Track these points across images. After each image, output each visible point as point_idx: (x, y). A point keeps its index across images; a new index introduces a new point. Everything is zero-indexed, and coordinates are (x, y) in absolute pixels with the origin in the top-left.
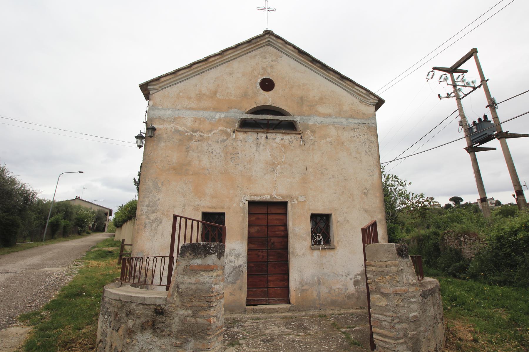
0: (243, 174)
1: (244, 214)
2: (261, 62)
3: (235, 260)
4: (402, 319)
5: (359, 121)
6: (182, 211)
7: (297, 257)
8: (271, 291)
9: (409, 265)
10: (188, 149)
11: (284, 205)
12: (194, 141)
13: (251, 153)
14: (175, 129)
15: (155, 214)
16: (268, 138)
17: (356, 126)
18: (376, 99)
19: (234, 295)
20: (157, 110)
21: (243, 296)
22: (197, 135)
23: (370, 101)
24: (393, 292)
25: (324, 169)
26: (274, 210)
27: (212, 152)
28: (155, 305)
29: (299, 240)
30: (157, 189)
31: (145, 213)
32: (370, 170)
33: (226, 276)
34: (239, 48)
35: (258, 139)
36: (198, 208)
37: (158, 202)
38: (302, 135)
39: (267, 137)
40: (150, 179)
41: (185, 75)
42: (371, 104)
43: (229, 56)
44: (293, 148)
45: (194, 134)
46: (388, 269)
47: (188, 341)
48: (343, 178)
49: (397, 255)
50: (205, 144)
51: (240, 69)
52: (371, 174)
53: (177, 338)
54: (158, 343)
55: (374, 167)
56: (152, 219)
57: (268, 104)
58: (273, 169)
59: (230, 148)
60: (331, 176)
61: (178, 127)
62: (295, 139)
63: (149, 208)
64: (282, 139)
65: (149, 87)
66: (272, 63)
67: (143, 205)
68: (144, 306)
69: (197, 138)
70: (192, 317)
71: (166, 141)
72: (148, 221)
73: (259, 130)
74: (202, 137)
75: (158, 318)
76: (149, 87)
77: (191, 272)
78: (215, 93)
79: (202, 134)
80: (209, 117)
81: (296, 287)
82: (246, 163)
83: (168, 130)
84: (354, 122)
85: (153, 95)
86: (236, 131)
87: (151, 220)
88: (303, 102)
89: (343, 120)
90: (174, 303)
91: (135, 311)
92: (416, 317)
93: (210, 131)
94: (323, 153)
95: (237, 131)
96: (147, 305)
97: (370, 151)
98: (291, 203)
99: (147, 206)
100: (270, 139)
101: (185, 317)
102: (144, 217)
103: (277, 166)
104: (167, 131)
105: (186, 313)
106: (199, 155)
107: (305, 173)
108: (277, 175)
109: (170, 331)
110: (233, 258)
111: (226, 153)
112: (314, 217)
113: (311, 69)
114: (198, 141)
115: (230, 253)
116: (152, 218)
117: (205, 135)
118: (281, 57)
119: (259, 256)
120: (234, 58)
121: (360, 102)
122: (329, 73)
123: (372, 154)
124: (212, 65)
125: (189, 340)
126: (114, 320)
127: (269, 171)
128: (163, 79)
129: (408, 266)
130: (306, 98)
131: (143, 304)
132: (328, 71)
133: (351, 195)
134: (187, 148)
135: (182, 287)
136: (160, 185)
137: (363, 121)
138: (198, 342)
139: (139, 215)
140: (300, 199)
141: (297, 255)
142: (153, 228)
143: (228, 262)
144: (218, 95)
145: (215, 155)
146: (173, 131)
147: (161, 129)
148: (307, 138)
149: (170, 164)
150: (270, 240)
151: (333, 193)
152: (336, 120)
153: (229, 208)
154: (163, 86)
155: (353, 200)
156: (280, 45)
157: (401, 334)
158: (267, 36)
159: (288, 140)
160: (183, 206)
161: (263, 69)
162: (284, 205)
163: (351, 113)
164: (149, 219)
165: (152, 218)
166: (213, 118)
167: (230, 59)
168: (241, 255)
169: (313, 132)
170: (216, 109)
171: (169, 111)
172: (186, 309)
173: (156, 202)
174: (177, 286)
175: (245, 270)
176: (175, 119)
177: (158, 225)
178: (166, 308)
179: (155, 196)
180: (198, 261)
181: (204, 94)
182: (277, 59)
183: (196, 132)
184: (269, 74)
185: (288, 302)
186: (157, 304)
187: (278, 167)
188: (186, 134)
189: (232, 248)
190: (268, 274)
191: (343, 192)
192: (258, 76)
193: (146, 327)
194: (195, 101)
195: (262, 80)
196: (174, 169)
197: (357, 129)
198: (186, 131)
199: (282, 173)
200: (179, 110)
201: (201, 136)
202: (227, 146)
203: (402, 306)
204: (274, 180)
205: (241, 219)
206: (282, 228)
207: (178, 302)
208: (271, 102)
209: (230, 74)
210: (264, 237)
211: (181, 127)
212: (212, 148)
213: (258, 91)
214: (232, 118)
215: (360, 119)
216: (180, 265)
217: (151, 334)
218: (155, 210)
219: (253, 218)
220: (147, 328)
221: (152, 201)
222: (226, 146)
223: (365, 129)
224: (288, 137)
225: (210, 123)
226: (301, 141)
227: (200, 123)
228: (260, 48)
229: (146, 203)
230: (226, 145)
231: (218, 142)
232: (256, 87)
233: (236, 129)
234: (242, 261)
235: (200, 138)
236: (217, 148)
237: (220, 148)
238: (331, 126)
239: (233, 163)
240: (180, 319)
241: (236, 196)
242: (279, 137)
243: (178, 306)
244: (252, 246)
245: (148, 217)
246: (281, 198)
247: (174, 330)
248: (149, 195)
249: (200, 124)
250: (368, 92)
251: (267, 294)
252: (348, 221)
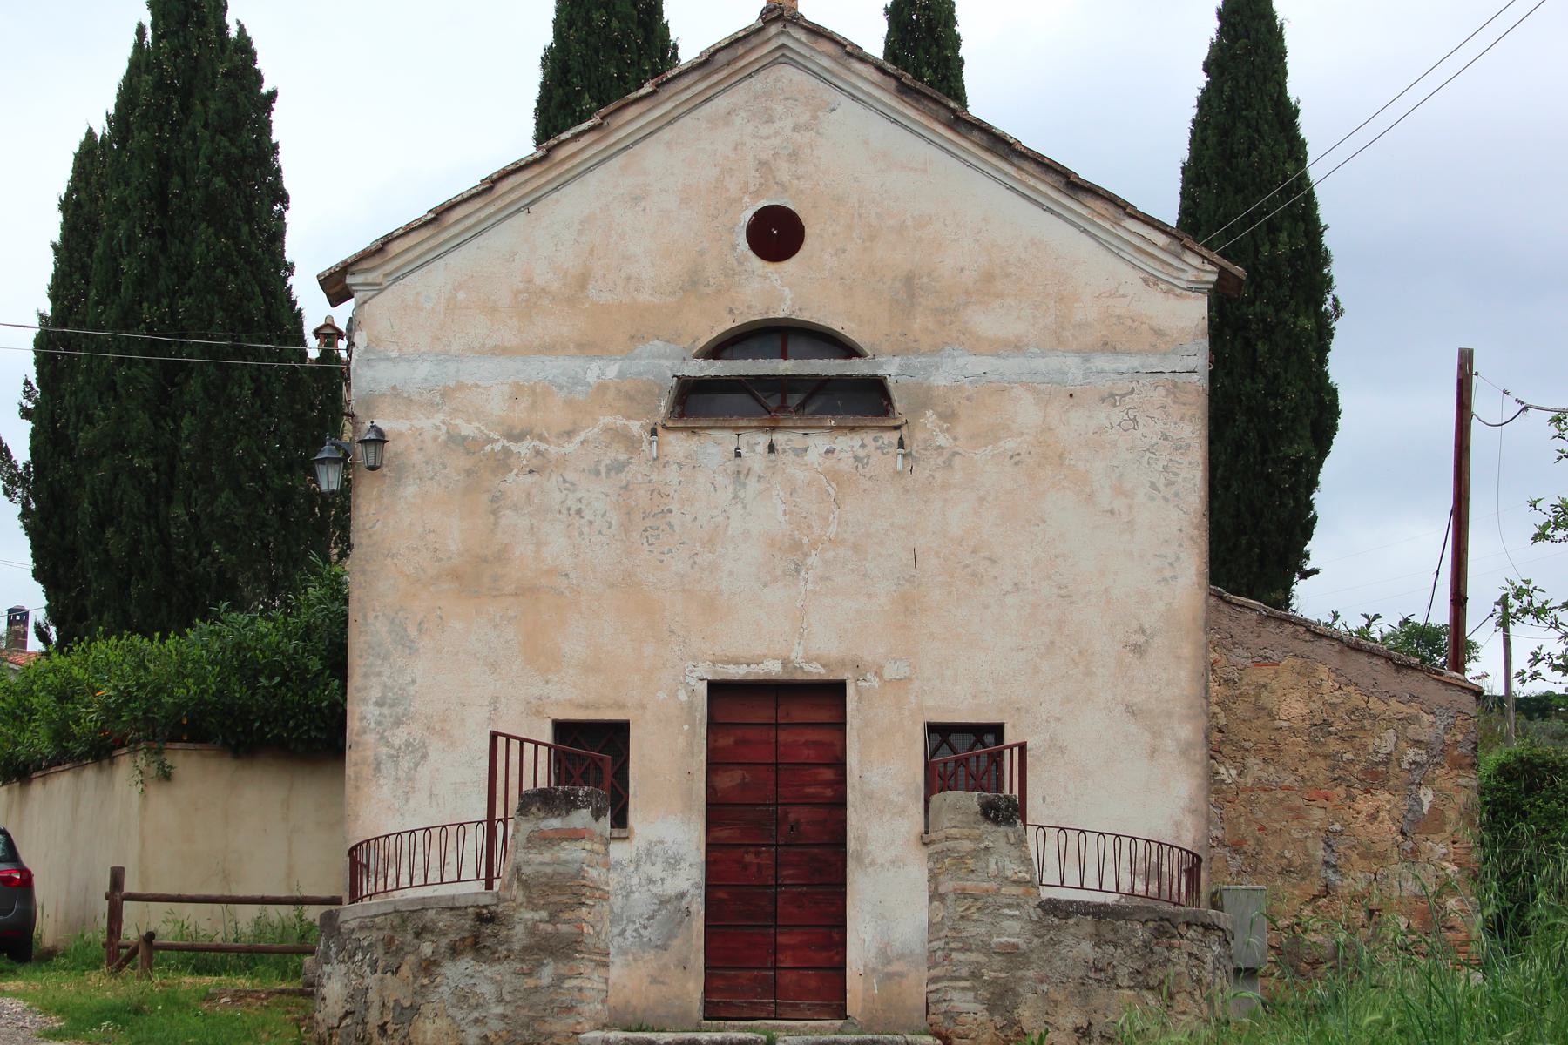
0: (687, 587)
1: (692, 725)
2: (754, 136)
3: (664, 875)
4: (971, 944)
5: (1135, 362)
6: (489, 718)
7: (870, 870)
8: (788, 978)
9: (1012, 840)
10: (497, 502)
11: (835, 691)
12: (517, 475)
13: (716, 508)
14: (448, 432)
15: (403, 728)
16: (778, 447)
17: (1120, 384)
18: (1209, 267)
19: (663, 983)
20: (382, 365)
21: (693, 988)
22: (524, 448)
23: (1185, 276)
24: (955, 890)
25: (985, 558)
26: (799, 712)
27: (579, 512)
28: (478, 906)
29: (881, 812)
30: (403, 645)
31: (373, 725)
32: (1165, 557)
33: (637, 925)
34: (667, 95)
35: (738, 455)
36: (539, 706)
37: (412, 689)
38: (904, 431)
39: (772, 448)
40: (380, 614)
41: (473, 220)
42: (1190, 289)
43: (629, 129)
44: (868, 484)
45: (514, 447)
46: (950, 844)
47: (542, 964)
48: (1055, 591)
49: (980, 817)
50: (553, 482)
51: (672, 174)
52: (1168, 573)
53: (523, 961)
54: (488, 973)
55: (1180, 546)
56: (397, 746)
57: (780, 314)
58: (792, 566)
59: (642, 493)
60: (1009, 587)
61: (459, 422)
62: (877, 448)
63: (386, 711)
64: (829, 451)
65: (349, 280)
66: (796, 137)
67: (365, 701)
68: (453, 912)
69: (524, 462)
70: (547, 922)
71: (421, 479)
72: (384, 750)
73: (742, 423)
74: (542, 455)
75: (483, 929)
76: (349, 280)
77: (543, 842)
78: (583, 281)
79: (543, 446)
80: (562, 380)
81: (865, 966)
82: (698, 548)
83: (428, 436)
84: (1114, 366)
85: (366, 306)
86: (659, 429)
87: (392, 747)
88: (913, 296)
89: (1072, 363)
90: (513, 901)
91: (435, 924)
92: (1016, 946)
93: (570, 434)
94: (982, 500)
95: (664, 427)
96: (459, 908)
97: (1169, 484)
98: (856, 685)
99: (380, 703)
100: (784, 451)
101: (536, 923)
102: (371, 738)
103: (806, 555)
104: (422, 441)
105: (537, 917)
106: (534, 521)
107: (913, 576)
108: (810, 587)
109: (509, 950)
110: (657, 871)
111: (628, 513)
112: (939, 733)
113: (949, 152)
114: (531, 472)
115: (649, 855)
116: (397, 743)
117: (553, 450)
118: (833, 110)
119: (746, 867)
120: (648, 130)
121: (1146, 282)
122: (1020, 168)
123: (1177, 495)
124: (567, 171)
125: (545, 962)
126: (386, 953)
127: (778, 572)
128: (395, 247)
129: (1008, 841)
130: (925, 280)
131: (452, 909)
132: (1015, 160)
133: (1080, 653)
134: (495, 499)
135: (526, 870)
136: (413, 632)
137: (1154, 362)
138: (560, 965)
139: (355, 732)
140: (890, 672)
141: (873, 863)
142: (400, 773)
143: (643, 882)
144: (591, 290)
145: (591, 523)
146: (443, 437)
147: (401, 434)
148: (925, 441)
149: (441, 560)
150: (786, 814)
151: (1012, 650)
152: (1039, 364)
153: (642, 706)
154: (397, 270)
155: (1089, 673)
156: (826, 62)
157: (965, 972)
158: (773, 29)
159: (850, 454)
160: (490, 703)
161: (762, 164)
162: (835, 691)
163: (1104, 333)
164: (388, 744)
165: (397, 743)
166: (577, 381)
167: (631, 140)
168: (684, 860)
169: (949, 417)
170: (588, 348)
171: (425, 364)
172: (536, 908)
173: (404, 690)
174: (518, 869)
175: (698, 907)
176: (446, 394)
177: (417, 765)
178: (499, 910)
179: (401, 671)
180: (555, 823)
181: (543, 290)
182: (815, 118)
183: (518, 438)
184: (782, 185)
185: (840, 1012)
186: (481, 904)
187: (813, 559)
188: (488, 448)
189: (655, 839)
190: (777, 926)
191: (1052, 643)
192: (742, 198)
193: (462, 948)
194: (511, 318)
195: (756, 214)
196: (456, 575)
197: (1123, 396)
198: (488, 436)
199: (828, 578)
200: (457, 358)
201: (538, 453)
202: (631, 487)
203: (976, 921)
204: (799, 605)
205: (681, 742)
206: (828, 774)
207: (521, 898)
208: (789, 303)
209: (636, 200)
210: (765, 805)
211: (468, 422)
212: (579, 494)
213: (740, 263)
214: (645, 378)
215: (1139, 352)
216: (517, 830)
217: (473, 959)
218: (404, 715)
219: (727, 741)
220: (465, 950)
221: (391, 689)
222: (626, 487)
223: (1155, 394)
224: (851, 443)
225: (569, 403)
226: (900, 457)
227: (534, 403)
228: (750, 76)
229: (375, 694)
230: (628, 482)
231: (598, 473)
232: (734, 247)
233: (658, 420)
234: (689, 878)
235: (537, 462)
236: (597, 496)
237: (607, 495)
238: (1019, 391)
239: (651, 548)
240: (526, 928)
241: (664, 665)
242: (818, 443)
243: (521, 904)
244: (722, 834)
245: (382, 737)
246: (823, 671)
247: (517, 946)
248: (382, 665)
249: (533, 406)
250: (1176, 242)
251: (775, 989)
252: (1062, 750)
